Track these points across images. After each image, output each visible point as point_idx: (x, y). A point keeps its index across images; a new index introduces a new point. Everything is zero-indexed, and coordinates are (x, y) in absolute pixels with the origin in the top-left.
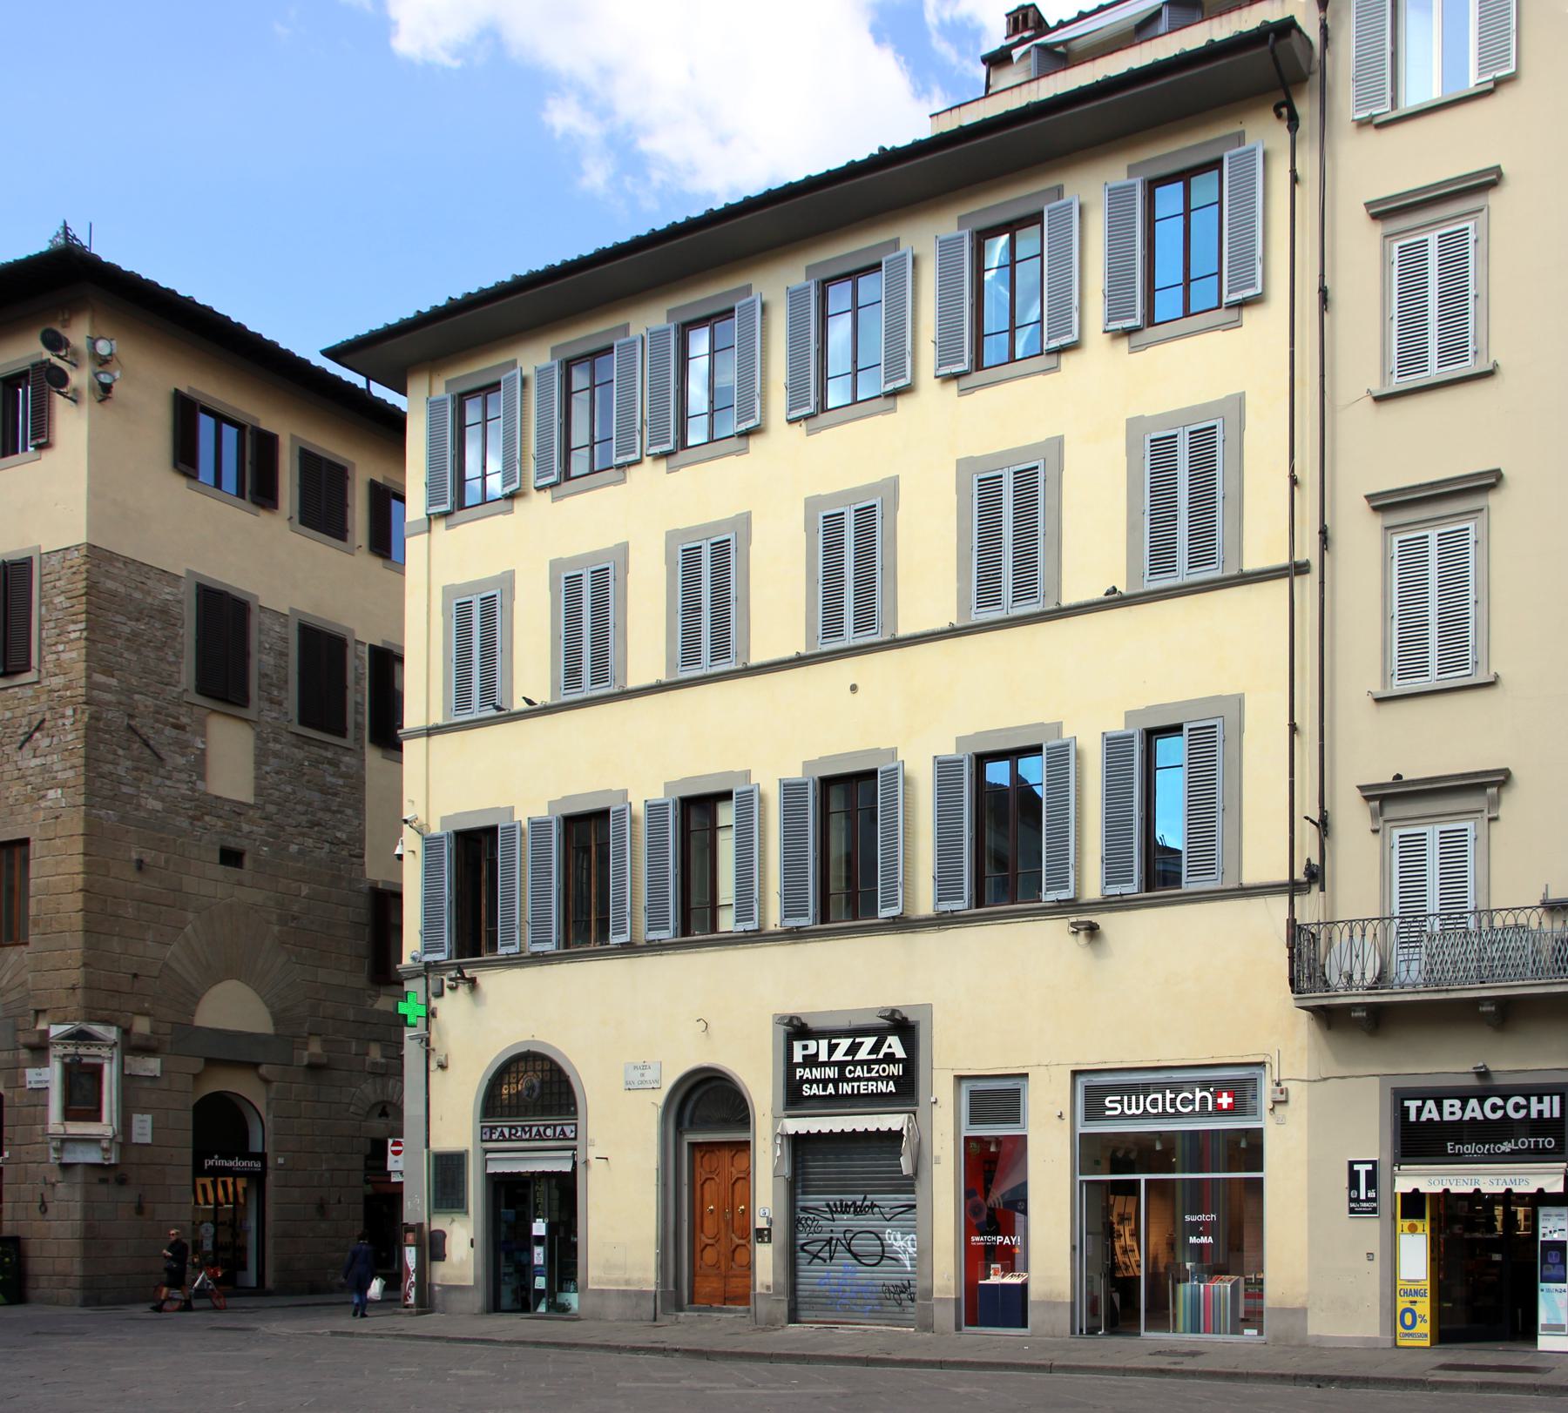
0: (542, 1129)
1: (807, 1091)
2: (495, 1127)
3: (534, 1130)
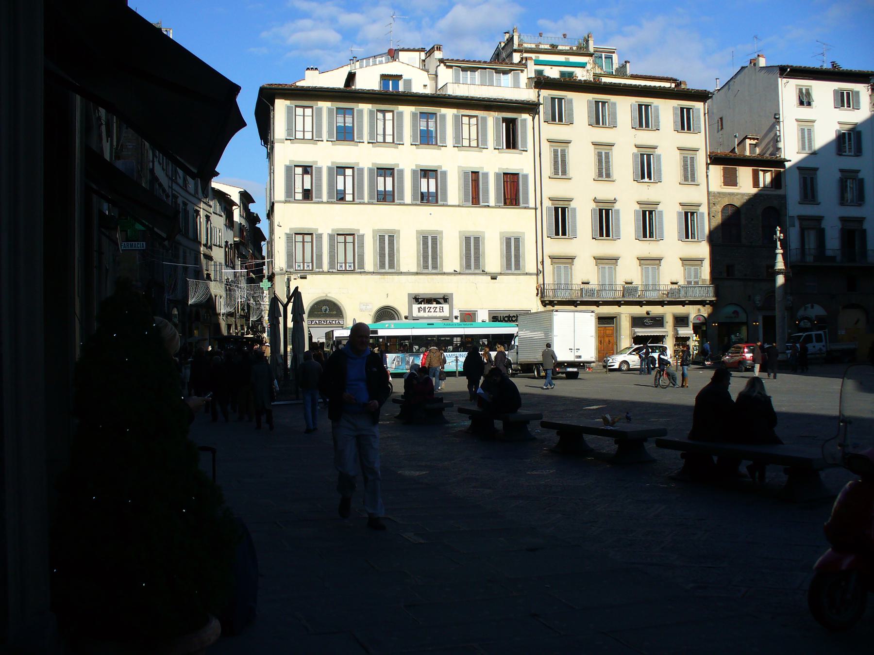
0: (331, 321)
1: (340, 179)
2: (313, 321)
3: (328, 322)
